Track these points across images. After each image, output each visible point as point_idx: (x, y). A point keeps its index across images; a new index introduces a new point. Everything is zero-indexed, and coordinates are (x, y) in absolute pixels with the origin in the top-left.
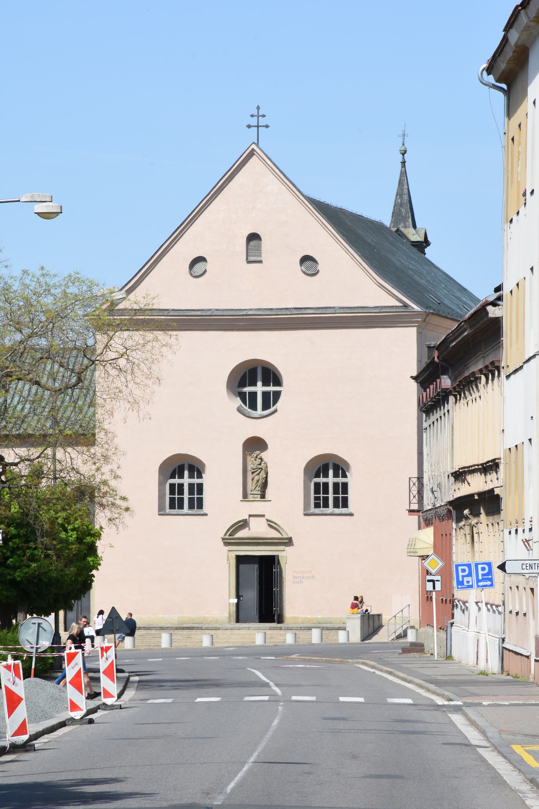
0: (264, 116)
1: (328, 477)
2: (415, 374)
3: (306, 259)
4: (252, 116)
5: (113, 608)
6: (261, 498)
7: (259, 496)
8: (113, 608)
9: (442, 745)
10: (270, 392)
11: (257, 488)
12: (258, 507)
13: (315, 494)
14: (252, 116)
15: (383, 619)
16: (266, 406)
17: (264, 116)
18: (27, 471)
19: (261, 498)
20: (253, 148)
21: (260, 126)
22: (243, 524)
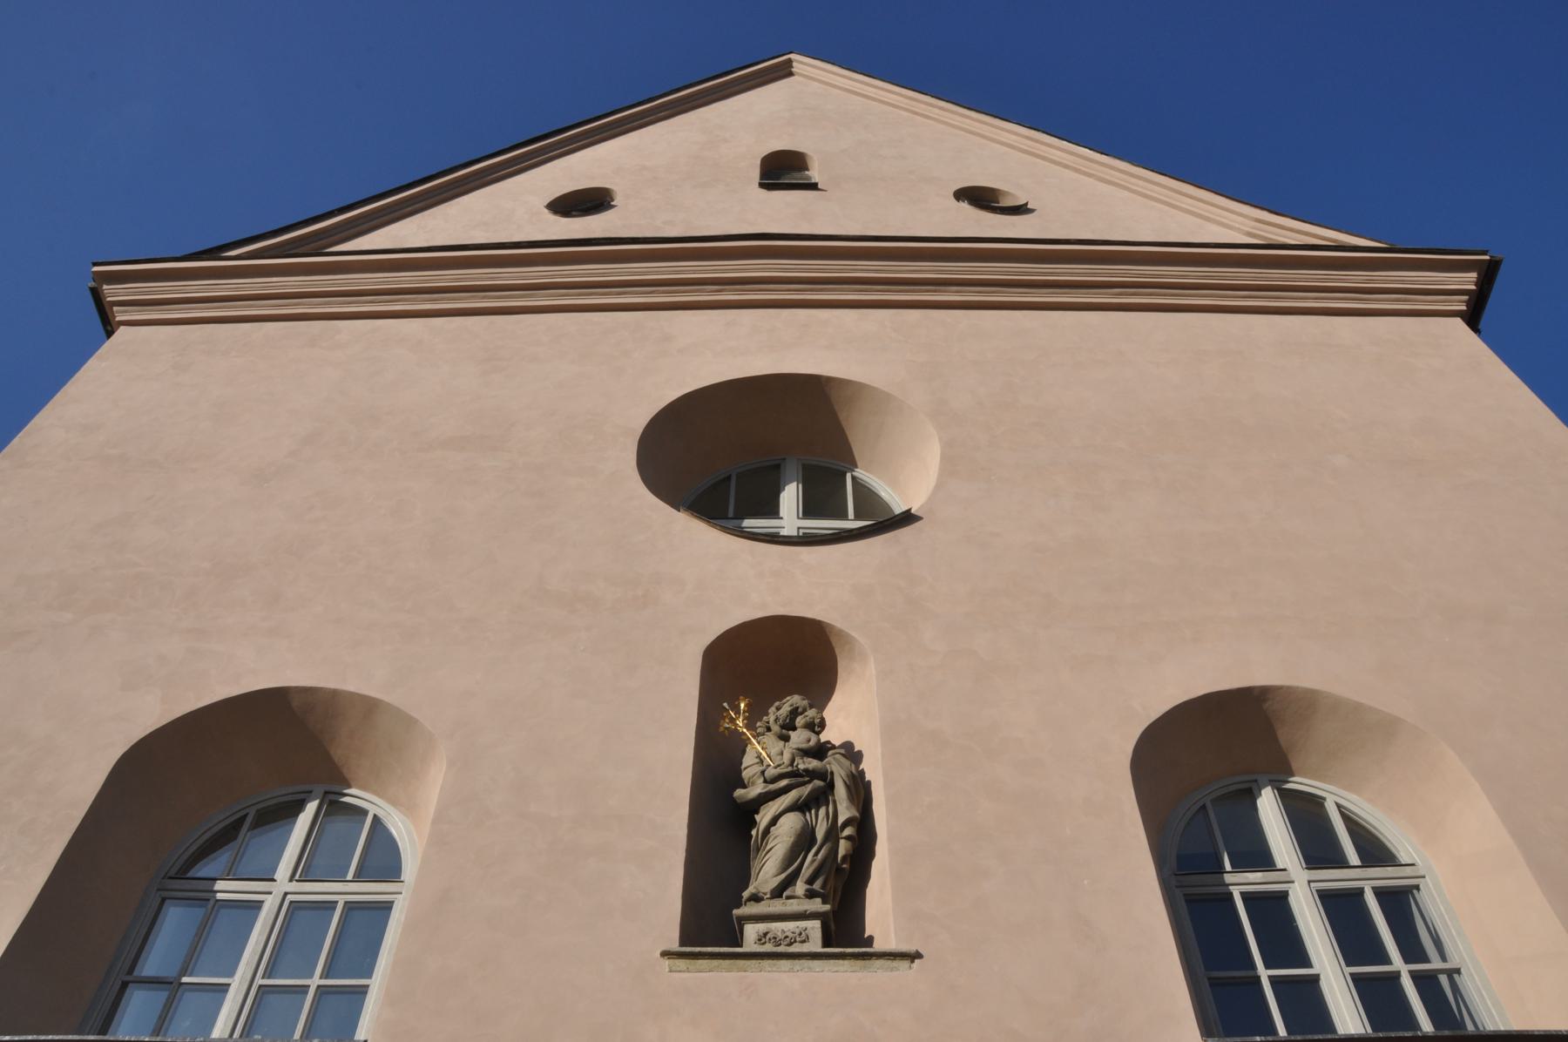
13: (1315, 979)
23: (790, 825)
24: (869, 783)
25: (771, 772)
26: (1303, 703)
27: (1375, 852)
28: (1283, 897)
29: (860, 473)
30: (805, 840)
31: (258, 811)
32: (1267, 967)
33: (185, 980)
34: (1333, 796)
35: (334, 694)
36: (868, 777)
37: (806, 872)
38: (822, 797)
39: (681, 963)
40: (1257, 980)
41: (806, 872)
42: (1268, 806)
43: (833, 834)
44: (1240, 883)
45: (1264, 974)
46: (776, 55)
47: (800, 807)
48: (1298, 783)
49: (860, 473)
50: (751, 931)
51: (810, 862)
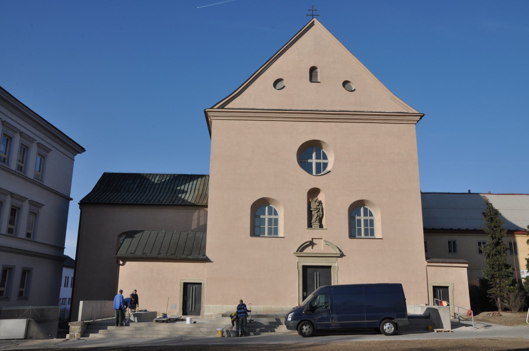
0: (316, 10)
1: (361, 216)
2: (71, 201)
3: (345, 83)
4: (309, 10)
5: (83, 150)
6: (320, 228)
7: (319, 226)
8: (83, 150)
9: (52, 150)
10: (321, 163)
11: (317, 221)
12: (315, 233)
13: (361, 228)
14: (309, 10)
15: (424, 312)
16: (318, 171)
17: (316, 10)
18: (481, 318)
19: (320, 228)
20: (24, 288)
21: (313, 14)
22: (311, 244)
23: (316, 215)
24: (323, 225)
25: (314, 208)
26: (367, 201)
27: (371, 215)
28: (361, 220)
29: (323, 150)
30: (318, 216)
31: (302, 252)
32: (357, 227)
33: (261, 226)
34: (369, 208)
35: (270, 198)
36: (322, 202)
37: (317, 220)
38: (319, 211)
39: (308, 229)
40: (356, 228)
41: (317, 220)
42: (362, 209)
43: (320, 215)
44: (357, 218)
45: (357, 227)
46: (310, 20)
47: (317, 212)
48: (366, 207)
49: (323, 150)
50: (313, 226)
51: (318, 218)
